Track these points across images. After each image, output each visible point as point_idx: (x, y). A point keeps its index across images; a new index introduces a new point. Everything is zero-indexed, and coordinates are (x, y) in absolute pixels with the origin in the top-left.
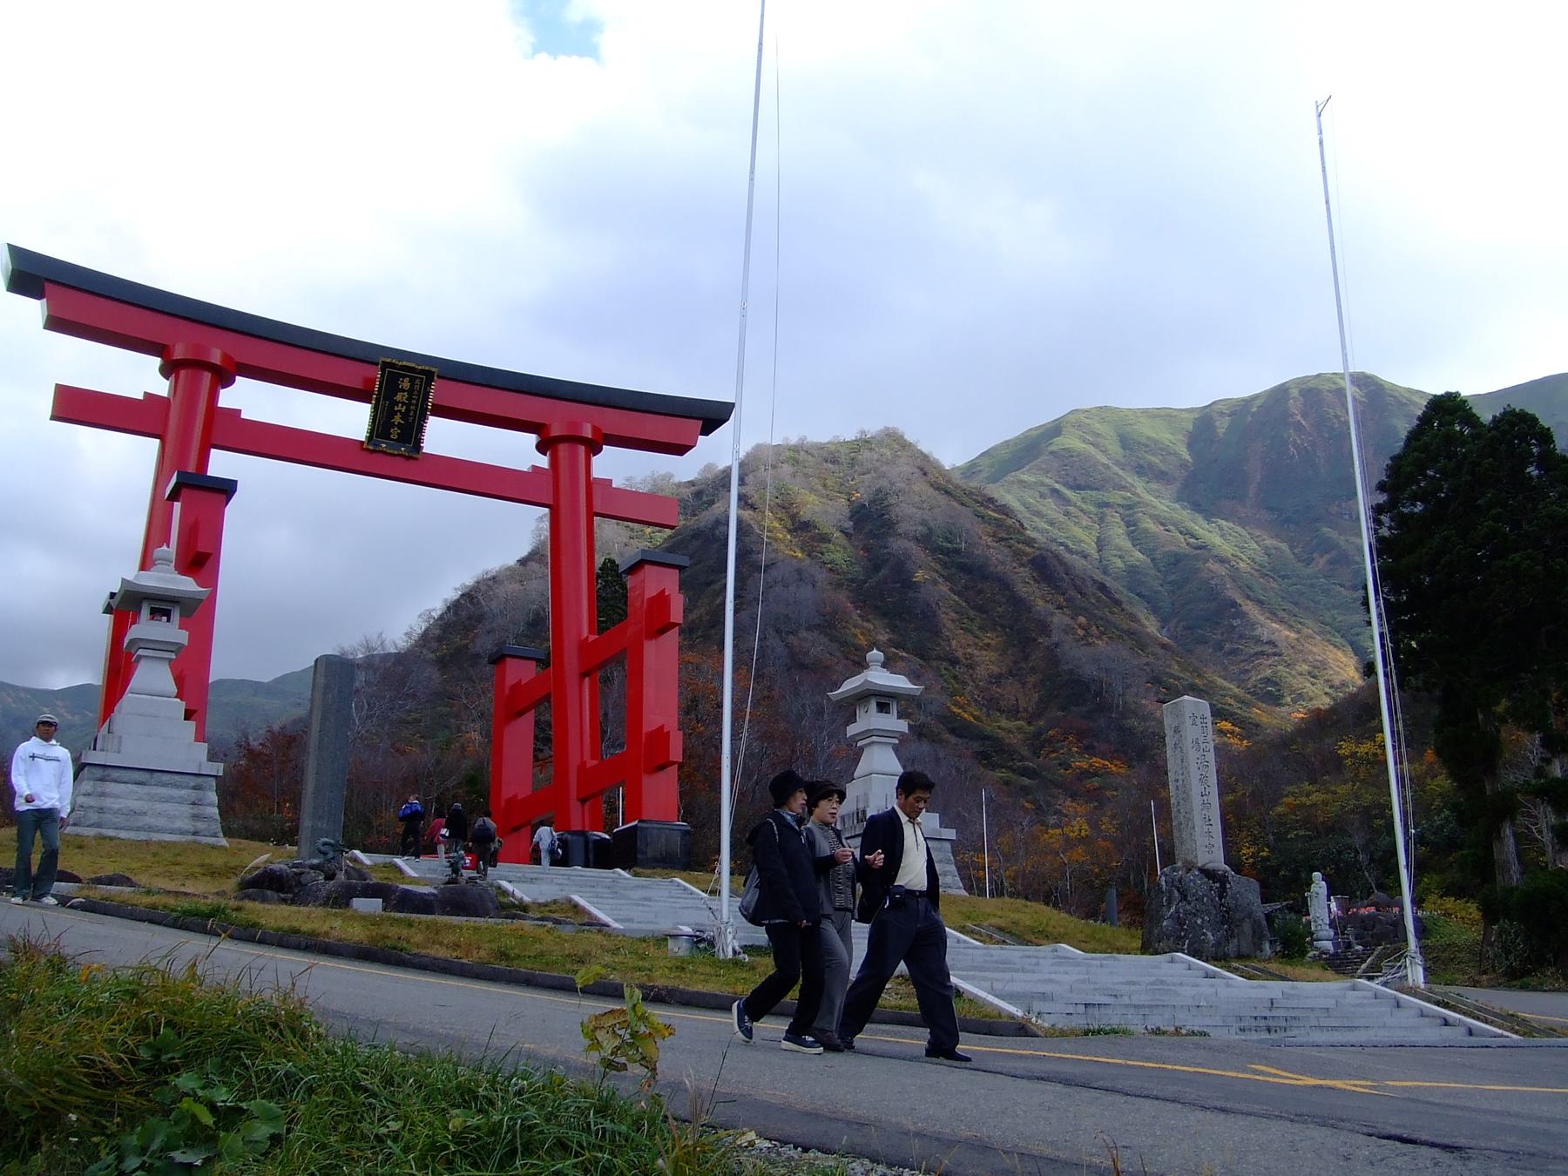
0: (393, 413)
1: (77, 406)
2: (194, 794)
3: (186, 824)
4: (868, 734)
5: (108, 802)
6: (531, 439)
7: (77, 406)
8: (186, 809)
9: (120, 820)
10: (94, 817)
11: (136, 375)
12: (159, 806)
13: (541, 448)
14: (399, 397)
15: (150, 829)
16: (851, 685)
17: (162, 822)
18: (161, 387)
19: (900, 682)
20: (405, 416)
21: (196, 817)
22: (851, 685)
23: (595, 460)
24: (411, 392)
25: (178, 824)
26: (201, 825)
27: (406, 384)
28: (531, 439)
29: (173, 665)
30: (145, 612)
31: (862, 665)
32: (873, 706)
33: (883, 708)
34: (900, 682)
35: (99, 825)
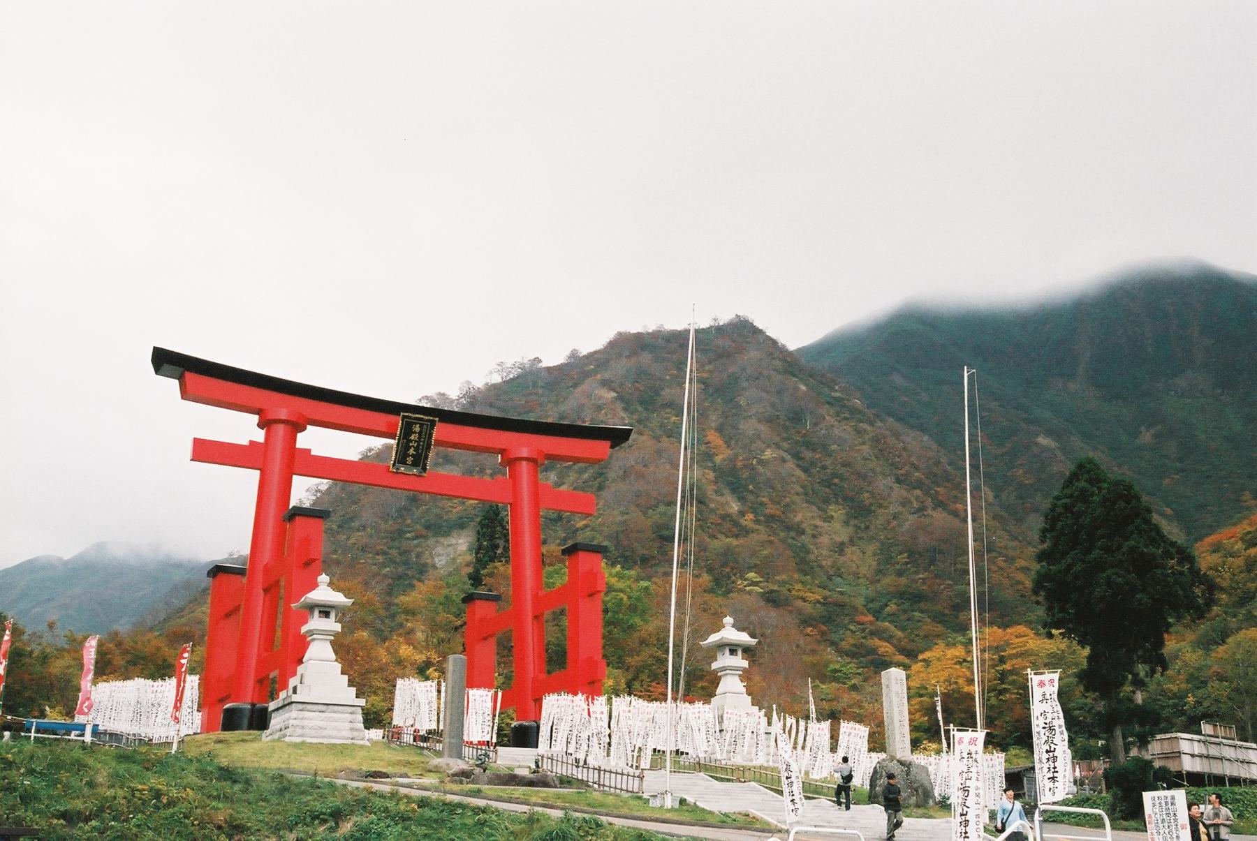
0: (409, 448)
1: (206, 451)
2: (350, 717)
3: (349, 734)
4: (724, 669)
5: (305, 723)
6: (256, 418)
7: (206, 451)
8: (349, 725)
9: (313, 733)
10: (299, 731)
11: (241, 428)
12: (333, 724)
13: (260, 425)
14: (412, 437)
15: (330, 737)
16: (713, 638)
17: (334, 733)
18: (260, 436)
19: (338, 598)
20: (416, 449)
21: (352, 729)
22: (713, 638)
23: (299, 435)
24: (420, 434)
25: (344, 734)
26: (355, 734)
27: (417, 429)
28: (256, 418)
29: (333, 644)
30: (316, 613)
31: (718, 627)
32: (727, 652)
33: (733, 652)
34: (338, 598)
35: (302, 736)
